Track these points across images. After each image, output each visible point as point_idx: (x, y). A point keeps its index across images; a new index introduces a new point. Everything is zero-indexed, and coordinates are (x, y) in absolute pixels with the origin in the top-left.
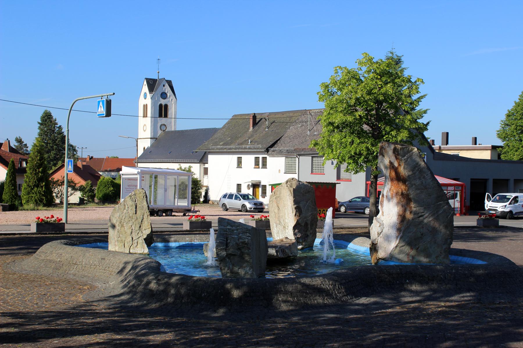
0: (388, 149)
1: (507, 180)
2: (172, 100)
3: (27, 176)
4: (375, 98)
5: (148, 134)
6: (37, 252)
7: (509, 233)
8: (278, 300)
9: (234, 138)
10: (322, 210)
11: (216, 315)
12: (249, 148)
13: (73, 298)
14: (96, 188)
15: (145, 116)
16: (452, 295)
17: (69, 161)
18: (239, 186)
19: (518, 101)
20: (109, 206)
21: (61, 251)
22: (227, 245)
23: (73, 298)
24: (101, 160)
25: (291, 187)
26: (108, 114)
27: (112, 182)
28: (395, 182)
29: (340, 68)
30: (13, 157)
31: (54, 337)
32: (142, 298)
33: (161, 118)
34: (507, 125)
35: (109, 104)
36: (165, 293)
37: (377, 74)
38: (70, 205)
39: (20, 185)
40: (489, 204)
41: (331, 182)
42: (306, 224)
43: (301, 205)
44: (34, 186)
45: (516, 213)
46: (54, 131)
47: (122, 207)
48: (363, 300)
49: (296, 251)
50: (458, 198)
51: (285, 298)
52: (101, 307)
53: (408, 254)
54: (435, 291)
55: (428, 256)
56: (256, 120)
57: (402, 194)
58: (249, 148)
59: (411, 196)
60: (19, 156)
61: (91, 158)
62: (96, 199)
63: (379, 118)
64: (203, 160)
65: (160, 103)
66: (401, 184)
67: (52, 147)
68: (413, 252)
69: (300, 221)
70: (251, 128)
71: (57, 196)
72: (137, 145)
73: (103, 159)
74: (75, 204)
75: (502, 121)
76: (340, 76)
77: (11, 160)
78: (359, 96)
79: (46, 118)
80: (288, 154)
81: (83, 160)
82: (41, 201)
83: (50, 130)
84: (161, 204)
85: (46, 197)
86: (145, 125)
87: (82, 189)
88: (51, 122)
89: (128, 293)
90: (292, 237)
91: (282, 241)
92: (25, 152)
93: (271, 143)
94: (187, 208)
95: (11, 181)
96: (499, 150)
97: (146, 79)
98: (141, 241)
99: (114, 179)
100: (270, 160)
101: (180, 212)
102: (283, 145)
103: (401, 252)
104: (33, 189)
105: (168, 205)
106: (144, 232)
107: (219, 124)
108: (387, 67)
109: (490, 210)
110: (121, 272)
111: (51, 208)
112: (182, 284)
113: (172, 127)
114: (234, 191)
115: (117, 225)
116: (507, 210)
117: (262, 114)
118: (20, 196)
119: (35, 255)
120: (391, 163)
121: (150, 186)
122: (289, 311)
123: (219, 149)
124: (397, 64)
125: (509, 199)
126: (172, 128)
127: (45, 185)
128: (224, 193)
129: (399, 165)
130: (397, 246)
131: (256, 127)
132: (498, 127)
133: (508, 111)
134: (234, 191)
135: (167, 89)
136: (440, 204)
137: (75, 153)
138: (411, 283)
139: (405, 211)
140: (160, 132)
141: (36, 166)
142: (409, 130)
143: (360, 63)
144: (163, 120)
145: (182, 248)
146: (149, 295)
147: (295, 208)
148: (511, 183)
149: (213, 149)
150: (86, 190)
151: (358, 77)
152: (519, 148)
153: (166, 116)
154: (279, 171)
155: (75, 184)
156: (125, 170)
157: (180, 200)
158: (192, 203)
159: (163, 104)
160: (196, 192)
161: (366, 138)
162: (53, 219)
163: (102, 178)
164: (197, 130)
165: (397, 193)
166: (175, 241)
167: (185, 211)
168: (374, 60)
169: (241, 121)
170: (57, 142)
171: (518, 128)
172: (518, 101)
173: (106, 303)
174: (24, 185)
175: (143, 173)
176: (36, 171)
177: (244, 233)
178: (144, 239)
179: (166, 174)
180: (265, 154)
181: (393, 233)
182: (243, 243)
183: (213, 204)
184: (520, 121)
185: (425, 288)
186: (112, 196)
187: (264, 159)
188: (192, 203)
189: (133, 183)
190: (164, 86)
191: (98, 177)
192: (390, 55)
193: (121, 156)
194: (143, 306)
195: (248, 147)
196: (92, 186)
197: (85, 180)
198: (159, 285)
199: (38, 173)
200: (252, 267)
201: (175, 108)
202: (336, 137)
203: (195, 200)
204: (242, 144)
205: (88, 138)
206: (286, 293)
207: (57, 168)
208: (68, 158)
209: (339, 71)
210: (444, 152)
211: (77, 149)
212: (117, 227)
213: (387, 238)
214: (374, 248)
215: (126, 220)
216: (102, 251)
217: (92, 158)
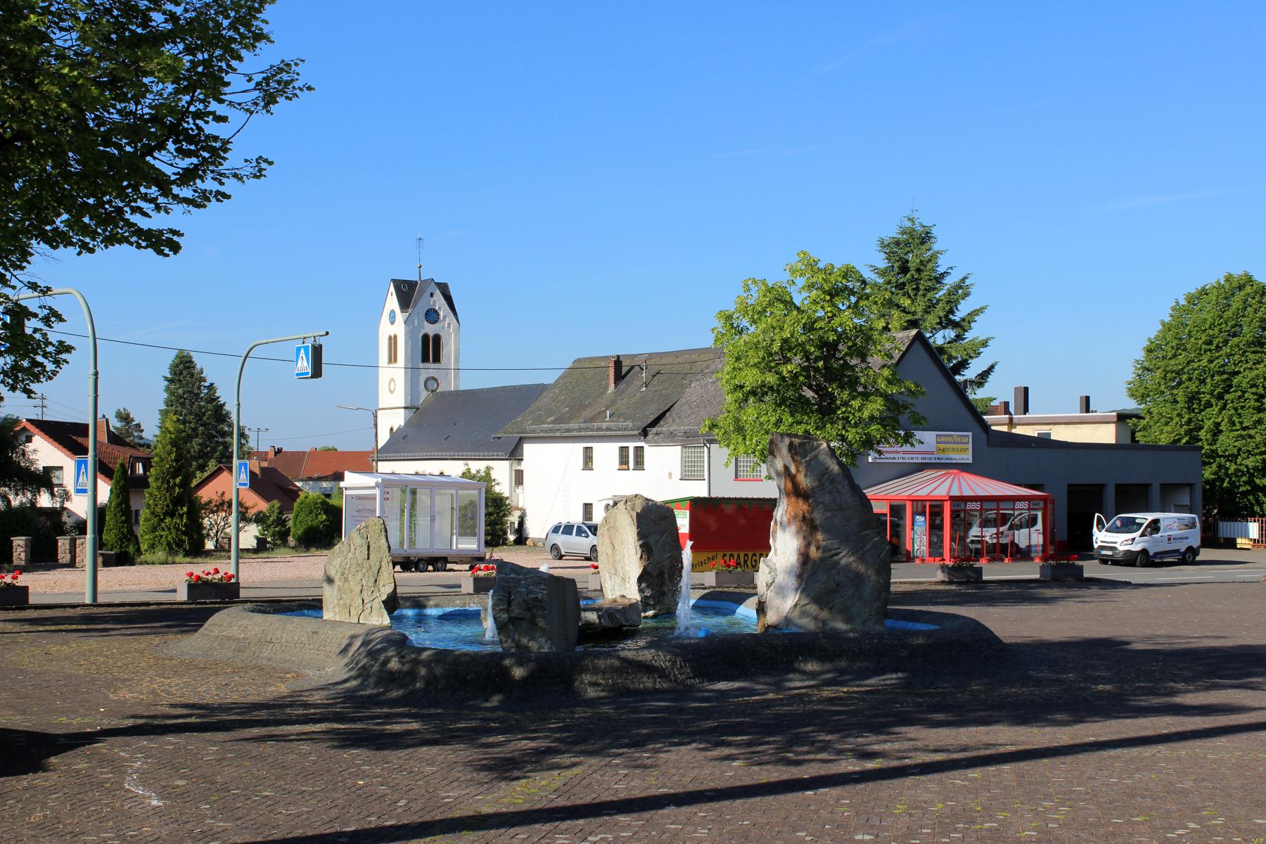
0: (781, 445)
1: (1146, 487)
3: (151, 494)
4: (821, 338)
5: (400, 399)
6: (206, 625)
7: (1094, 590)
8: (582, 682)
9: (576, 408)
10: (750, 554)
11: (488, 705)
12: (608, 429)
13: (273, 689)
14: (291, 516)
15: (393, 358)
16: (867, 678)
17: (241, 465)
18: (588, 508)
19: (1168, 319)
20: (319, 553)
21: (246, 622)
22: (509, 604)
23: (273, 689)
24: (298, 456)
25: (633, 509)
26: (317, 372)
27: (324, 503)
28: (793, 499)
29: (754, 282)
30: (121, 456)
31: (252, 726)
32: (377, 685)
34: (1148, 370)
35: (317, 352)
36: (412, 674)
37: (824, 292)
38: (242, 552)
39: (137, 512)
40: (1101, 537)
41: (749, 496)
42: (661, 573)
43: (651, 540)
44: (166, 514)
45: (1156, 554)
46: (197, 395)
47: (345, 548)
48: (722, 685)
49: (635, 618)
50: (1039, 525)
51: (594, 679)
52: (317, 698)
53: (816, 618)
54: (842, 672)
55: (848, 620)
56: (621, 371)
57: (804, 518)
58: (608, 429)
59: (817, 522)
60: (129, 452)
61: (278, 452)
62: (290, 538)
63: (831, 375)
64: (515, 454)
65: (423, 332)
66: (801, 502)
67: (195, 430)
68: (824, 614)
69: (649, 569)
70: (612, 386)
71: (208, 535)
72: (376, 425)
73: (304, 453)
74: (248, 550)
75: (1137, 361)
76: (755, 297)
77: (120, 461)
78: (787, 334)
79: (181, 367)
80: (687, 439)
81: (262, 456)
82: (180, 544)
83: (190, 392)
84: (423, 546)
85: (190, 537)
86: (392, 380)
87: (260, 519)
88: (192, 375)
89: (355, 678)
90: (633, 594)
91: (615, 601)
92: (137, 440)
93: (652, 418)
94: (477, 555)
95: (119, 505)
96: (1130, 422)
97: (394, 281)
98: (378, 604)
99: (328, 496)
100: (650, 452)
101: (462, 562)
102: (678, 420)
103: (804, 614)
104: (162, 520)
105: (439, 548)
106: (382, 589)
107: (549, 378)
108: (844, 277)
109: (1102, 548)
110: (345, 650)
111: (199, 560)
112: (437, 661)
113: (451, 383)
114: (577, 518)
115: (336, 579)
116: (1136, 548)
117: (635, 356)
118: (136, 537)
119: (196, 635)
120: (786, 468)
121: (403, 511)
122: (599, 698)
123: (546, 431)
124: (922, 243)
125: (1141, 525)
127: (188, 513)
128: (555, 523)
129: (798, 471)
130: (796, 605)
131: (622, 385)
132: (1129, 374)
133: (1150, 340)
134: (577, 518)
135: (439, 303)
136: (867, 535)
137: (243, 441)
138: (805, 661)
139: (808, 546)
140: (424, 394)
141: (168, 473)
142: (885, 396)
143: (793, 271)
144: (430, 369)
145: (444, 618)
146: (389, 679)
147: (641, 546)
148: (1155, 492)
149: (534, 431)
150: (269, 522)
151: (788, 298)
152: (1171, 419)
153: (437, 359)
154: (670, 474)
155: (247, 508)
156: (352, 479)
157: (462, 539)
158: (487, 544)
159: (431, 335)
160: (496, 519)
161: (807, 414)
162: (218, 576)
163: (302, 495)
164: (503, 388)
165: (795, 517)
166: (436, 606)
167: (474, 561)
168: (821, 265)
169: (591, 372)
170: (205, 418)
171: (1169, 375)
172: (1168, 319)
173: (325, 693)
174: (144, 513)
175: (387, 485)
176: (168, 482)
177: (535, 584)
179: (438, 485)
180: (640, 441)
181: (792, 582)
182: (536, 599)
183: (535, 545)
184: (1172, 362)
185: (828, 666)
186: (324, 531)
187: (639, 451)
188: (487, 544)
189: (367, 504)
190: (432, 295)
191: (294, 494)
192: (909, 224)
193: (344, 445)
194: (379, 694)
195: (604, 425)
196: (281, 513)
197: (268, 499)
198: (403, 664)
199: (173, 487)
200: (549, 638)
201: (457, 343)
202: (750, 412)
203: (495, 538)
204: (592, 420)
205: (273, 414)
206: (596, 670)
207: (206, 474)
208: (239, 458)
209: (752, 286)
210: (1019, 430)
211: (247, 432)
212: (337, 582)
213: (781, 591)
214: (761, 609)
215: (353, 570)
216: (314, 620)
217: (280, 451)
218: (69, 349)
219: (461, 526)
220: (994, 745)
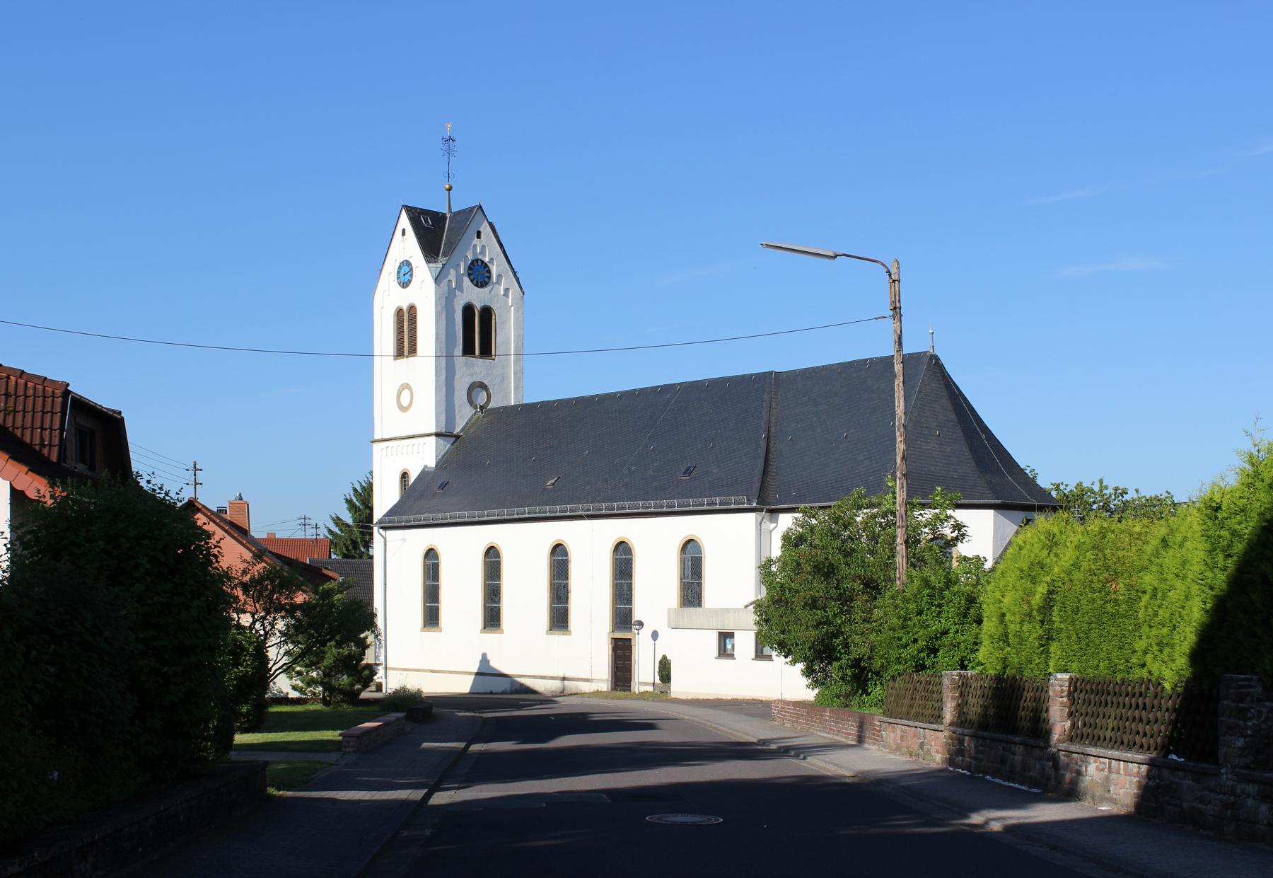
2: (507, 290)
5: (426, 416)
15: (406, 345)
126: (507, 395)
144: (477, 368)
153: (486, 351)
159: (478, 306)
190: (479, 235)
219: (936, 723)
220: (785, 752)
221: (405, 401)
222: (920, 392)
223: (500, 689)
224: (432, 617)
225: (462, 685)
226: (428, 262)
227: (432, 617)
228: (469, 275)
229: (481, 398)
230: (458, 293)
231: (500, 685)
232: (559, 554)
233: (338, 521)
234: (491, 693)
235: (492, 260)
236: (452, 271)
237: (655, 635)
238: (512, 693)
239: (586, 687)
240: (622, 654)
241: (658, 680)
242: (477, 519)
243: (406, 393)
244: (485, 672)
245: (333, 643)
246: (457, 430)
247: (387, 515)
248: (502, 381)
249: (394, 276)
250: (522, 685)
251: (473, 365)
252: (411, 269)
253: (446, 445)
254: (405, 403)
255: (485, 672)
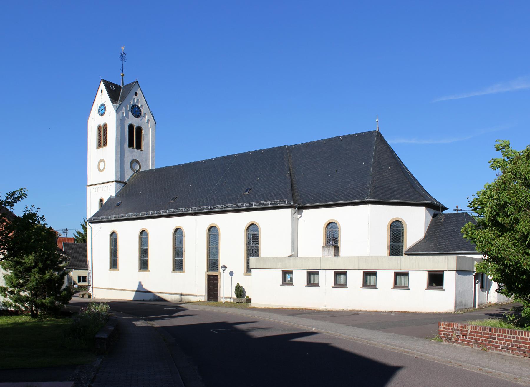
2: (148, 120)
5: (111, 173)
15: (102, 142)
33: (132, 149)
153: (139, 147)
159: (135, 126)
178: (496, 291)
190: (136, 94)
218: (43, 216)
221: (101, 167)
222: (376, 148)
223: (148, 299)
224: (114, 264)
225: (130, 296)
226: (113, 103)
227: (114, 264)
228: (132, 111)
229: (137, 167)
230: (126, 119)
231: (148, 297)
232: (178, 233)
233: (78, 232)
234: (144, 300)
235: (142, 106)
236: (124, 108)
237: (231, 273)
238: (154, 301)
239: (193, 299)
240: (213, 284)
241: (234, 296)
242: (136, 217)
243: (102, 163)
244: (141, 290)
245: (36, 270)
246: (125, 181)
247: (93, 217)
248: (146, 160)
249: (97, 111)
250: (159, 297)
251: (133, 152)
252: (105, 107)
253: (121, 187)
254: (101, 168)
255: (141, 290)
